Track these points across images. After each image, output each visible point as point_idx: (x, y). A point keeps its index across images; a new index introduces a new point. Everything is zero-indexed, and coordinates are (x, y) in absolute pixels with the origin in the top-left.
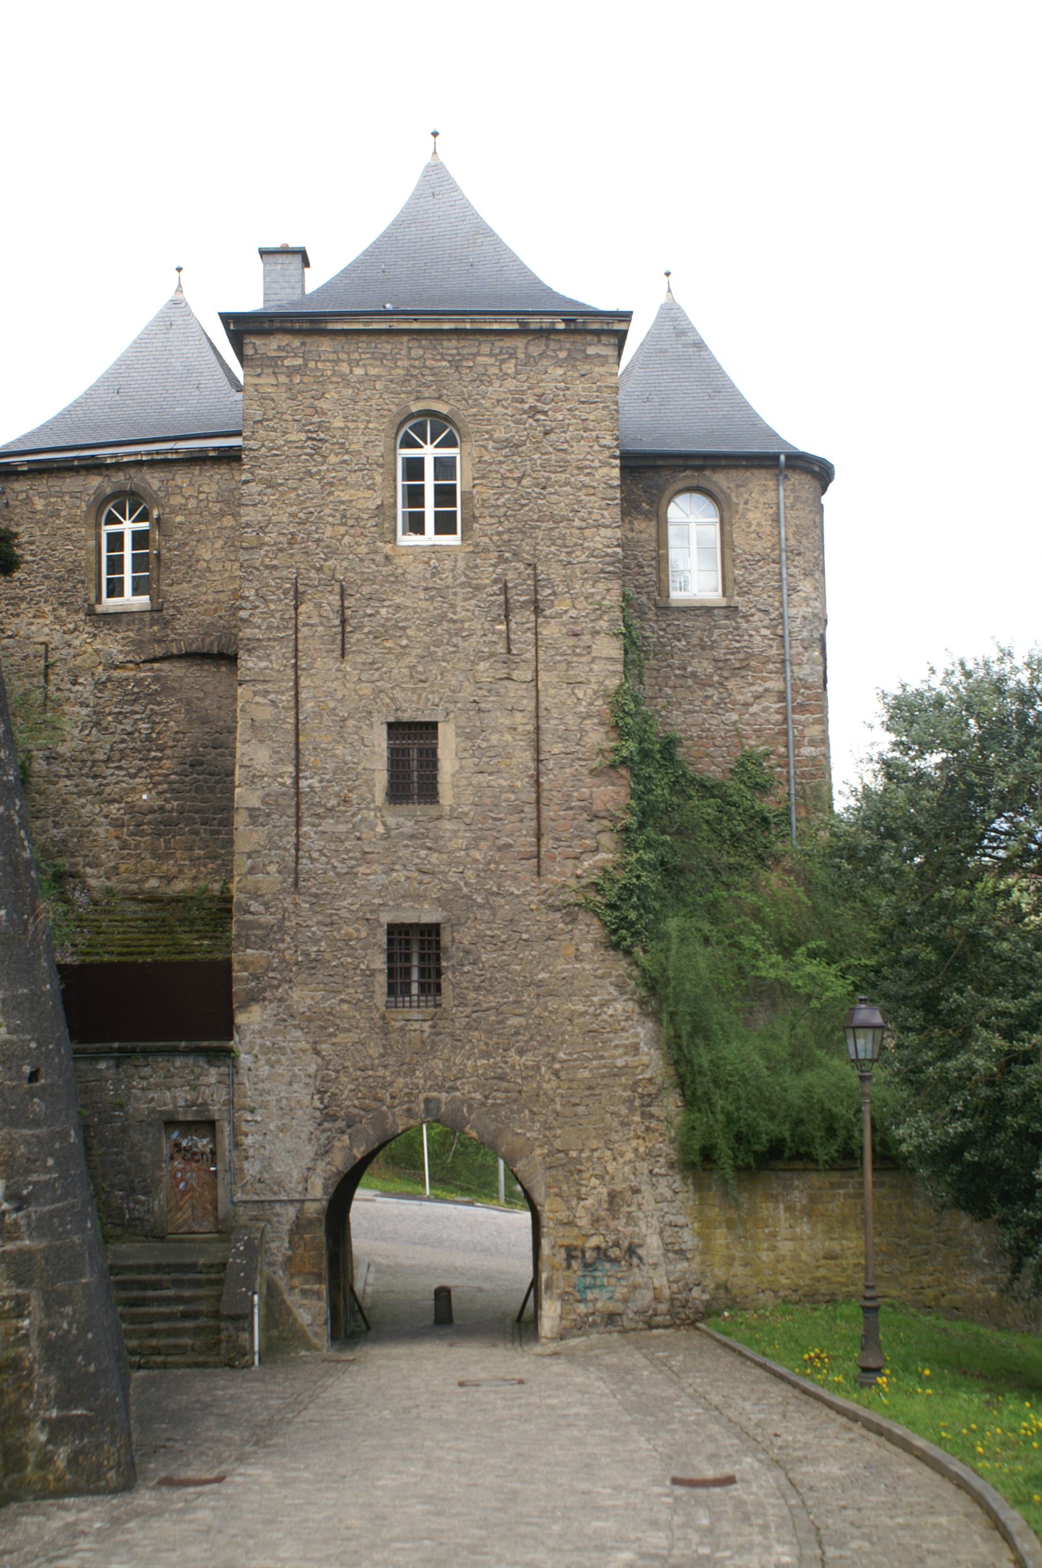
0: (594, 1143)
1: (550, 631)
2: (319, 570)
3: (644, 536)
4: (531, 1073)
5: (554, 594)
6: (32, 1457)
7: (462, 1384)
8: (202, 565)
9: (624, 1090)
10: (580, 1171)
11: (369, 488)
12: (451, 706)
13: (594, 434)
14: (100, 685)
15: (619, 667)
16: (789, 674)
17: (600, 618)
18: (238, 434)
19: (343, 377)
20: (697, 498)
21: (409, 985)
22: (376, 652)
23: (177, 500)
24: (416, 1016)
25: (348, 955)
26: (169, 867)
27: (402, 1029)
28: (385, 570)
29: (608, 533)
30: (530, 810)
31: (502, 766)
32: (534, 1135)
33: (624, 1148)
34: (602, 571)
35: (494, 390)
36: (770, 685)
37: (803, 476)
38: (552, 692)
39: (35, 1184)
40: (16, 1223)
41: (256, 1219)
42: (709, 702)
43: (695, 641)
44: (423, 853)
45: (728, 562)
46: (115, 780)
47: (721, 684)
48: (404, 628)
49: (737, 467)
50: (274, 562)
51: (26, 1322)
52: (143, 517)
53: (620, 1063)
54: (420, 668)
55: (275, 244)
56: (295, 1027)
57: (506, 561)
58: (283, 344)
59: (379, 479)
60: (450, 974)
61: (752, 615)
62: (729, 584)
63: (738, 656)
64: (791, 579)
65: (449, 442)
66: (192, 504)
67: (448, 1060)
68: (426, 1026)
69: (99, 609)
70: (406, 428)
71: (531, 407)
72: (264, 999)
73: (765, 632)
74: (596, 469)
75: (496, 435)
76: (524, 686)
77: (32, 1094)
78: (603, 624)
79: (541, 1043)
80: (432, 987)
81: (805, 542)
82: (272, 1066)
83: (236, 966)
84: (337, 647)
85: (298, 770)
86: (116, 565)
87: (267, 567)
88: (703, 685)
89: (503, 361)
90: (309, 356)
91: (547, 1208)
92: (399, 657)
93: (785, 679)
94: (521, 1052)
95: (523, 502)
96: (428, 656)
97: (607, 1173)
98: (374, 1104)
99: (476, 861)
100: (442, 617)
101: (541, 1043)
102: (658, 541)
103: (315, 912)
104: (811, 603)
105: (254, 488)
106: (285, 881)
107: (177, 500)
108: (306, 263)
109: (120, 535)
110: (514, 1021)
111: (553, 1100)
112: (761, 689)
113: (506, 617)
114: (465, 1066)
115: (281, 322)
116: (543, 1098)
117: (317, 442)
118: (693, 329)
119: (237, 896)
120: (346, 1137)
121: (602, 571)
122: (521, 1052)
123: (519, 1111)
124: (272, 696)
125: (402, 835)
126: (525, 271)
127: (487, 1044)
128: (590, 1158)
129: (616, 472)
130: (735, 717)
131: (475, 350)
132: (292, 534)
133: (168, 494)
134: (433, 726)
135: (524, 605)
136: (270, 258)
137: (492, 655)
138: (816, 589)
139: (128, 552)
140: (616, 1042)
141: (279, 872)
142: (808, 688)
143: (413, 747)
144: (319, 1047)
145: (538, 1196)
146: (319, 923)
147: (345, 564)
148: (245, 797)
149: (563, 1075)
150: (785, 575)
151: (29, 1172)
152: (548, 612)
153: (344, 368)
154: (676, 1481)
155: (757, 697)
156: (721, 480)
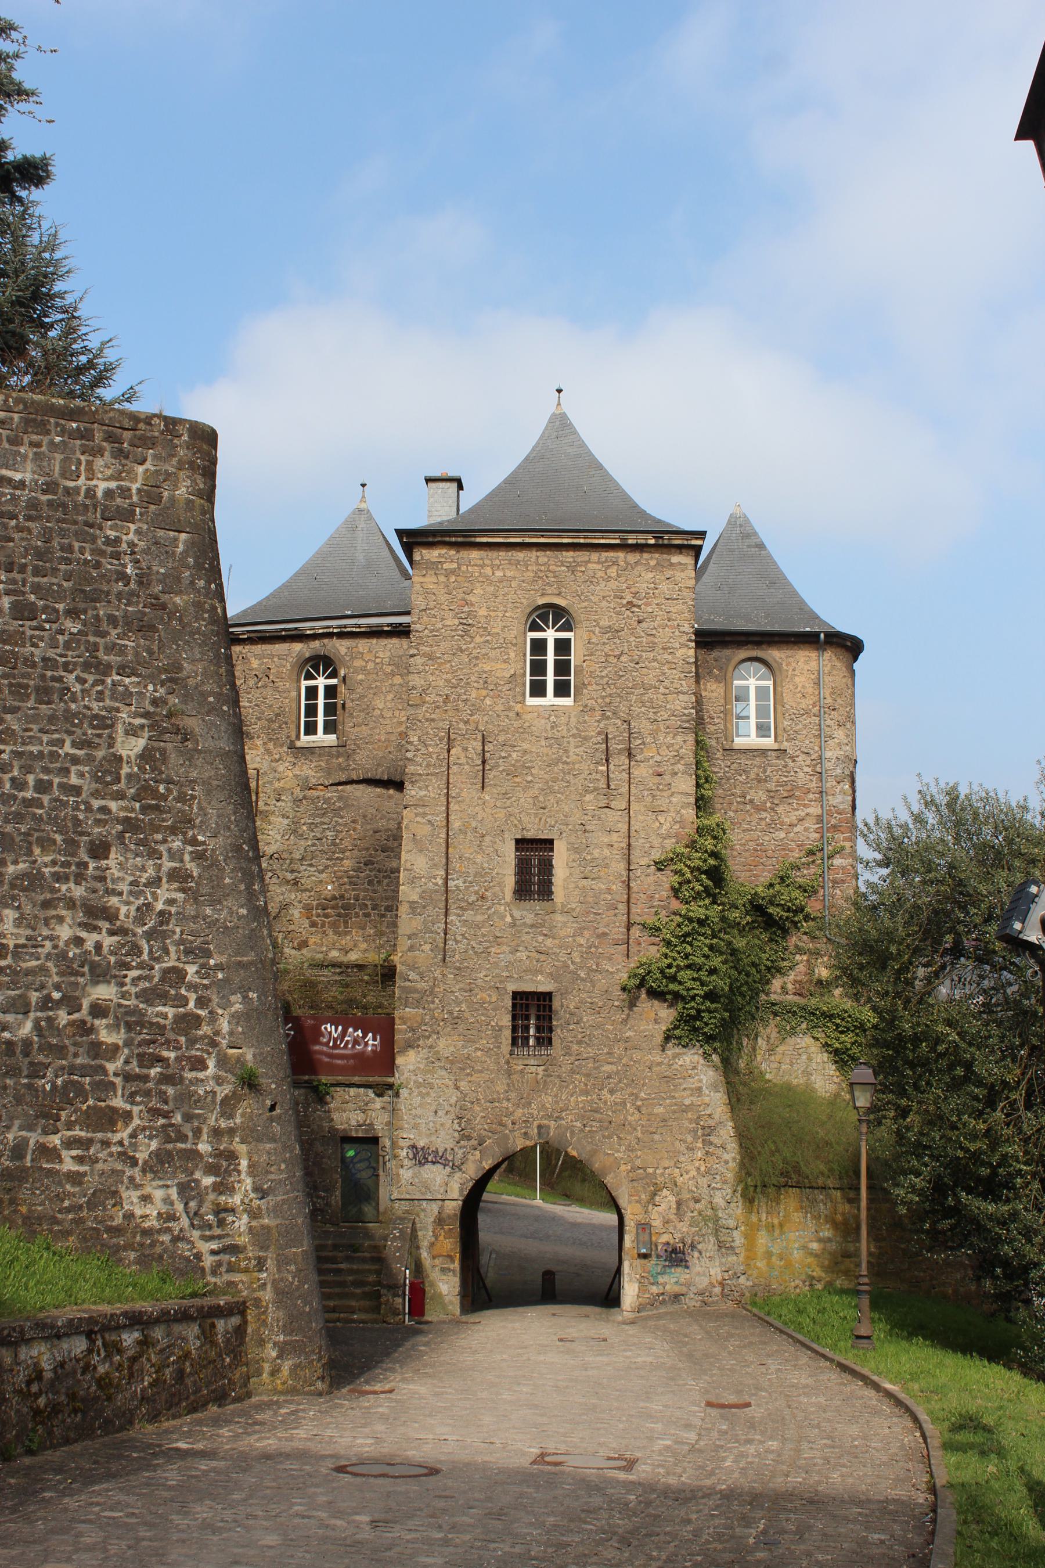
1: (641, 772)
2: (466, 723)
3: (715, 694)
5: (644, 743)
6: (267, 1367)
7: (561, 1340)
8: (377, 712)
11: (505, 662)
12: (563, 827)
14: (297, 801)
15: (692, 800)
17: (678, 762)
18: (408, 613)
19: (487, 578)
21: (527, 1039)
22: (507, 786)
23: (359, 663)
26: (346, 941)
27: (522, 1071)
28: (516, 724)
29: (686, 698)
30: (622, 908)
31: (602, 874)
32: (620, 1155)
33: (689, 1167)
34: (680, 727)
35: (602, 589)
38: (640, 817)
40: (259, 1208)
41: (407, 1212)
42: (763, 823)
44: (540, 938)
46: (309, 875)
47: (772, 809)
48: (530, 768)
49: (787, 643)
52: (333, 675)
53: (687, 1102)
54: (541, 798)
56: (441, 1068)
57: (608, 718)
59: (512, 655)
60: (559, 1031)
65: (567, 627)
66: (370, 666)
69: (298, 744)
70: (534, 616)
73: (806, 769)
77: (271, 1119)
78: (680, 767)
79: (627, 1085)
80: (545, 1040)
81: (839, 701)
83: (397, 1021)
85: (447, 874)
86: (311, 711)
87: (427, 720)
88: (759, 809)
89: (608, 567)
90: (461, 561)
92: (525, 789)
94: (612, 1092)
96: (548, 790)
100: (559, 760)
101: (627, 1085)
103: (458, 981)
105: (419, 660)
107: (359, 663)
108: (460, 487)
109: (316, 688)
110: (607, 1068)
113: (607, 760)
116: (627, 1127)
117: (466, 627)
118: (755, 534)
119: (400, 968)
121: (680, 727)
122: (612, 1092)
123: (610, 1137)
126: (625, 497)
128: (662, 1174)
129: (692, 652)
130: (782, 835)
131: (586, 558)
133: (352, 658)
134: (551, 842)
135: (620, 752)
137: (596, 789)
138: (847, 736)
139: (321, 701)
143: (534, 860)
145: (623, 1202)
146: (461, 989)
147: (486, 718)
148: (407, 892)
149: (644, 1110)
151: (268, 1172)
152: (638, 758)
153: (488, 571)
154: (709, 1404)
156: (775, 654)
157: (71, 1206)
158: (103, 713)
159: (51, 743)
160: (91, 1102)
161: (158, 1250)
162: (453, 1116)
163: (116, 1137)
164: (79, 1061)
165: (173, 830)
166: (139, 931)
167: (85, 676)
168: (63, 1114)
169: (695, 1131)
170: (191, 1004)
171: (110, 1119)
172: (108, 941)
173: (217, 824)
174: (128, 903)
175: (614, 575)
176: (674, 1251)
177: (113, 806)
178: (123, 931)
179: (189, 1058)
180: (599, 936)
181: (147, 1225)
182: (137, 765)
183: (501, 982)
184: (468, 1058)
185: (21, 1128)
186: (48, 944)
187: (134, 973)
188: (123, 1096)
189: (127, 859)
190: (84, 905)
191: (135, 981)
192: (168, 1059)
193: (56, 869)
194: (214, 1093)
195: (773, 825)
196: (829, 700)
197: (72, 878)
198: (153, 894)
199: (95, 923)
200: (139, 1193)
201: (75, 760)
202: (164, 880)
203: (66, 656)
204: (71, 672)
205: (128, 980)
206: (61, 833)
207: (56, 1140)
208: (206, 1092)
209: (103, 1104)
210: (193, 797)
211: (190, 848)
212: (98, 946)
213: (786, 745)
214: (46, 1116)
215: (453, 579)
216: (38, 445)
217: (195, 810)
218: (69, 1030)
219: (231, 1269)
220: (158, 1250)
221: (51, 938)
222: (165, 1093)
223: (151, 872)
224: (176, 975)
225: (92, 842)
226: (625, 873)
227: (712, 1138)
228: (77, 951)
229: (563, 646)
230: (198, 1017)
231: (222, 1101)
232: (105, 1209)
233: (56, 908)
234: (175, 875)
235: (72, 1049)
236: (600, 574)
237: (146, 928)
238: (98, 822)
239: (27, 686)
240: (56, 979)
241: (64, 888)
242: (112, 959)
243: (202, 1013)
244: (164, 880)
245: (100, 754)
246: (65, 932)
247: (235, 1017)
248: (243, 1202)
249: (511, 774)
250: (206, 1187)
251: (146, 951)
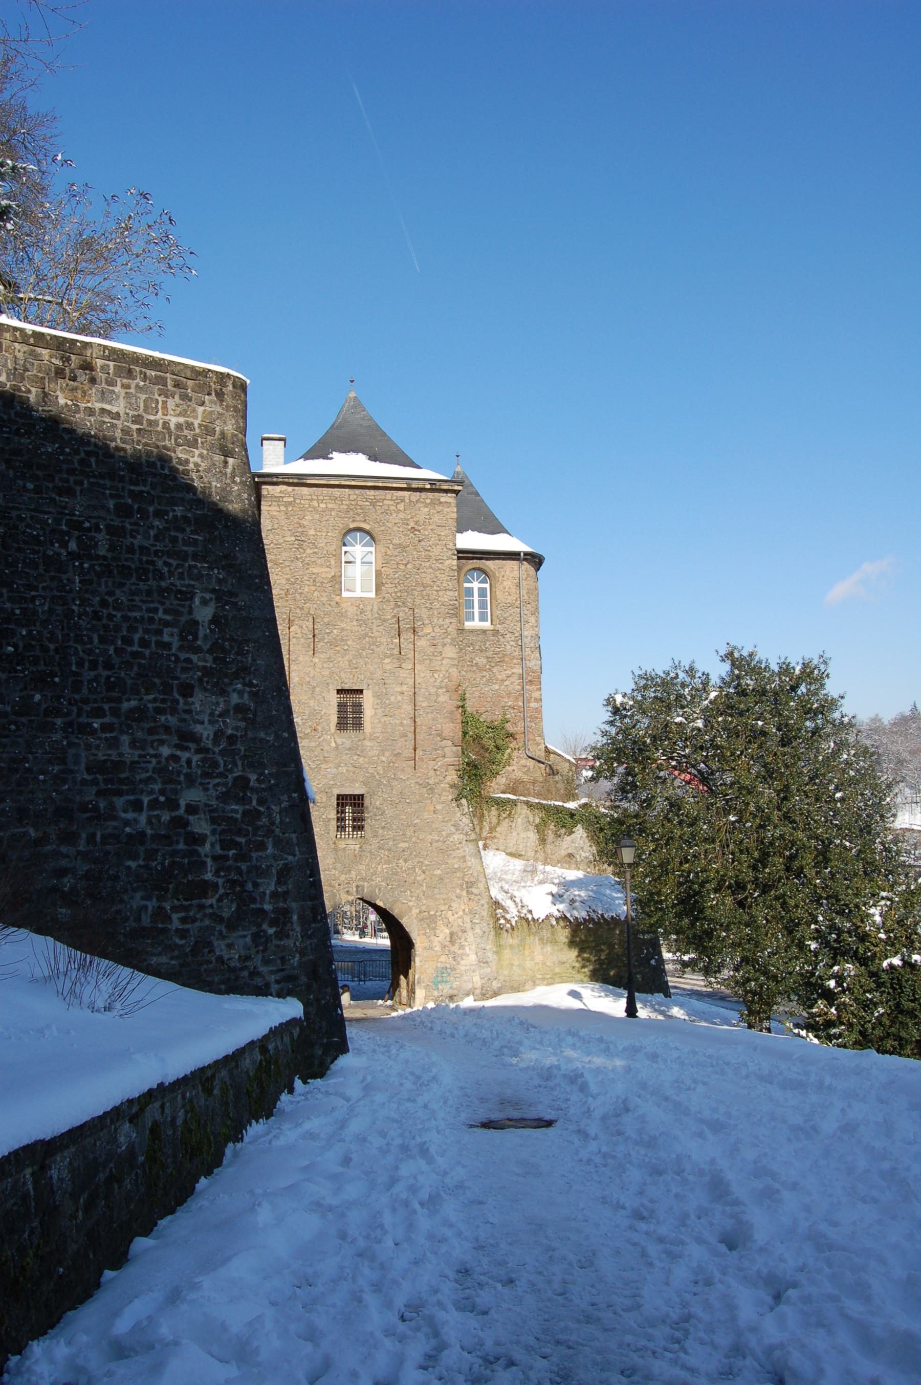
1: (422, 643)
2: (302, 609)
19: (314, 508)
27: (344, 849)
28: (336, 610)
29: (451, 593)
30: (411, 736)
34: (448, 613)
35: (394, 518)
36: (514, 670)
44: (355, 757)
53: (456, 866)
54: (354, 661)
57: (399, 606)
59: (333, 562)
73: (512, 643)
80: (358, 827)
88: (481, 669)
89: (398, 503)
94: (406, 861)
100: (366, 635)
110: (403, 845)
122: (406, 861)
129: (455, 562)
137: (392, 655)
152: (420, 634)
158: (184, 589)
159: (149, 610)
163: (209, 902)
166: (217, 750)
167: (170, 561)
169: (462, 885)
170: (254, 803)
171: (205, 888)
172: (195, 758)
175: (402, 508)
177: (194, 658)
178: (207, 750)
180: (395, 755)
181: (232, 965)
183: (329, 788)
185: (143, 898)
186: (154, 761)
190: (176, 731)
193: (158, 704)
195: (490, 681)
196: (526, 597)
197: (168, 712)
198: (224, 722)
199: (186, 744)
201: (167, 624)
202: (232, 712)
203: (155, 546)
204: (160, 557)
205: (211, 786)
211: (248, 689)
212: (189, 762)
213: (499, 627)
216: (128, 387)
221: (155, 756)
224: (243, 782)
226: (412, 712)
228: (175, 766)
232: (203, 955)
233: (158, 734)
236: (392, 508)
238: (184, 670)
239: (129, 568)
241: (163, 718)
243: (262, 809)
244: (232, 712)
245: (183, 619)
246: (165, 751)
249: (333, 644)
251: (222, 765)
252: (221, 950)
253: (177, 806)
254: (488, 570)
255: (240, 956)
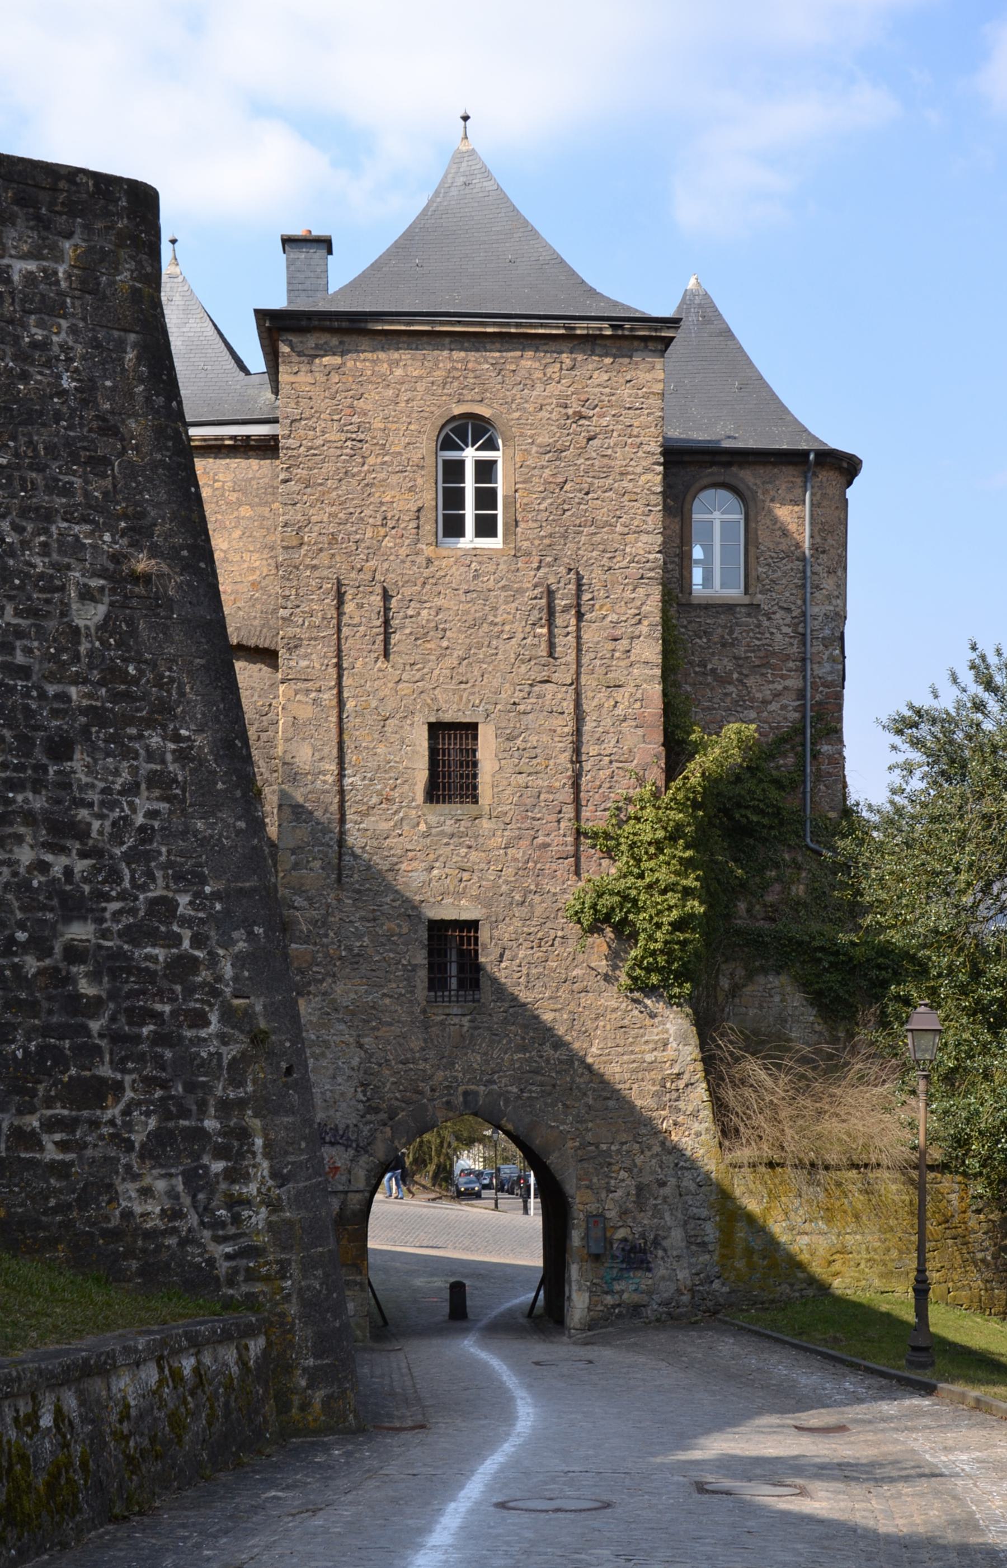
0: (624, 1137)
4: (565, 1067)
9: (654, 1085)
10: (610, 1164)
13: (638, 440)
15: (658, 672)
16: (809, 672)
19: (384, 377)
20: (723, 494)
24: (455, 1011)
25: (391, 950)
27: (442, 1023)
28: (427, 572)
30: (569, 811)
32: (567, 1128)
33: (652, 1141)
36: (789, 683)
37: (831, 473)
39: (293, 1163)
42: (728, 700)
43: (715, 638)
45: (752, 560)
47: (740, 681)
49: (765, 464)
50: (314, 562)
51: (289, 1283)
53: (649, 1057)
55: (297, 231)
56: (339, 1020)
58: (321, 342)
61: (774, 613)
62: (752, 581)
63: (759, 654)
64: (816, 577)
65: (490, 445)
67: (485, 1054)
68: (465, 1021)
70: (447, 430)
71: (575, 413)
72: (309, 993)
74: (640, 475)
75: (539, 440)
76: (564, 689)
81: (830, 541)
82: (317, 1059)
84: (379, 646)
91: (577, 1200)
93: (804, 677)
95: (566, 507)
97: (635, 1166)
98: (415, 1097)
99: (516, 860)
102: (682, 539)
103: (358, 908)
104: (834, 602)
106: (328, 877)
108: (330, 252)
111: (585, 1094)
112: (780, 687)
114: (503, 1059)
115: (320, 320)
116: (576, 1092)
120: (388, 1129)
123: (553, 1105)
124: (313, 695)
125: (442, 833)
127: (523, 1039)
128: (619, 1151)
132: (332, 534)
134: (473, 727)
135: (566, 610)
136: (301, 255)
138: (838, 586)
140: (646, 1038)
141: (323, 868)
142: (828, 687)
144: (363, 1041)
146: (362, 919)
150: (809, 574)
151: (286, 1153)
152: (587, 617)
155: (777, 695)
156: (748, 477)
157: (57, 1205)
160: (73, 1071)
161: (164, 1256)
162: (355, 1083)
163: (109, 1114)
164: (54, 1019)
165: (149, 723)
166: (117, 851)
168: (41, 1088)
170: (186, 944)
171: (99, 1092)
172: (81, 866)
173: (204, 714)
174: (101, 817)
176: (633, 1249)
179: (187, 1012)
182: (99, 639)
184: (373, 1008)
187: (115, 906)
188: (111, 1062)
189: (95, 761)
191: (117, 915)
192: (162, 1013)
194: (220, 1055)
198: (131, 804)
199: (62, 842)
200: (137, 1185)
201: (19, 633)
202: (143, 786)
206: (10, 727)
207: (34, 1122)
208: (210, 1054)
209: (87, 1073)
210: (172, 680)
211: (172, 746)
212: (68, 872)
214: (22, 1091)
215: (335, 378)
217: (175, 696)
218: (41, 982)
219: (251, 1276)
220: (164, 1256)
222: (162, 1056)
223: (125, 776)
224: (164, 908)
225: (50, 739)
227: (681, 1104)
228: (42, 879)
229: (485, 470)
230: (196, 959)
231: (229, 1065)
232: (99, 1208)
233: (11, 824)
234: (155, 780)
235: (45, 1004)
237: (124, 848)
238: (55, 713)
240: (19, 915)
241: (20, 798)
242: (87, 888)
243: (199, 954)
244: (143, 786)
246: (25, 855)
247: (239, 961)
248: (259, 1190)
250: (217, 1175)
252: (130, 1198)
253: (49, 953)
254: (741, 487)
255: (162, 1210)
